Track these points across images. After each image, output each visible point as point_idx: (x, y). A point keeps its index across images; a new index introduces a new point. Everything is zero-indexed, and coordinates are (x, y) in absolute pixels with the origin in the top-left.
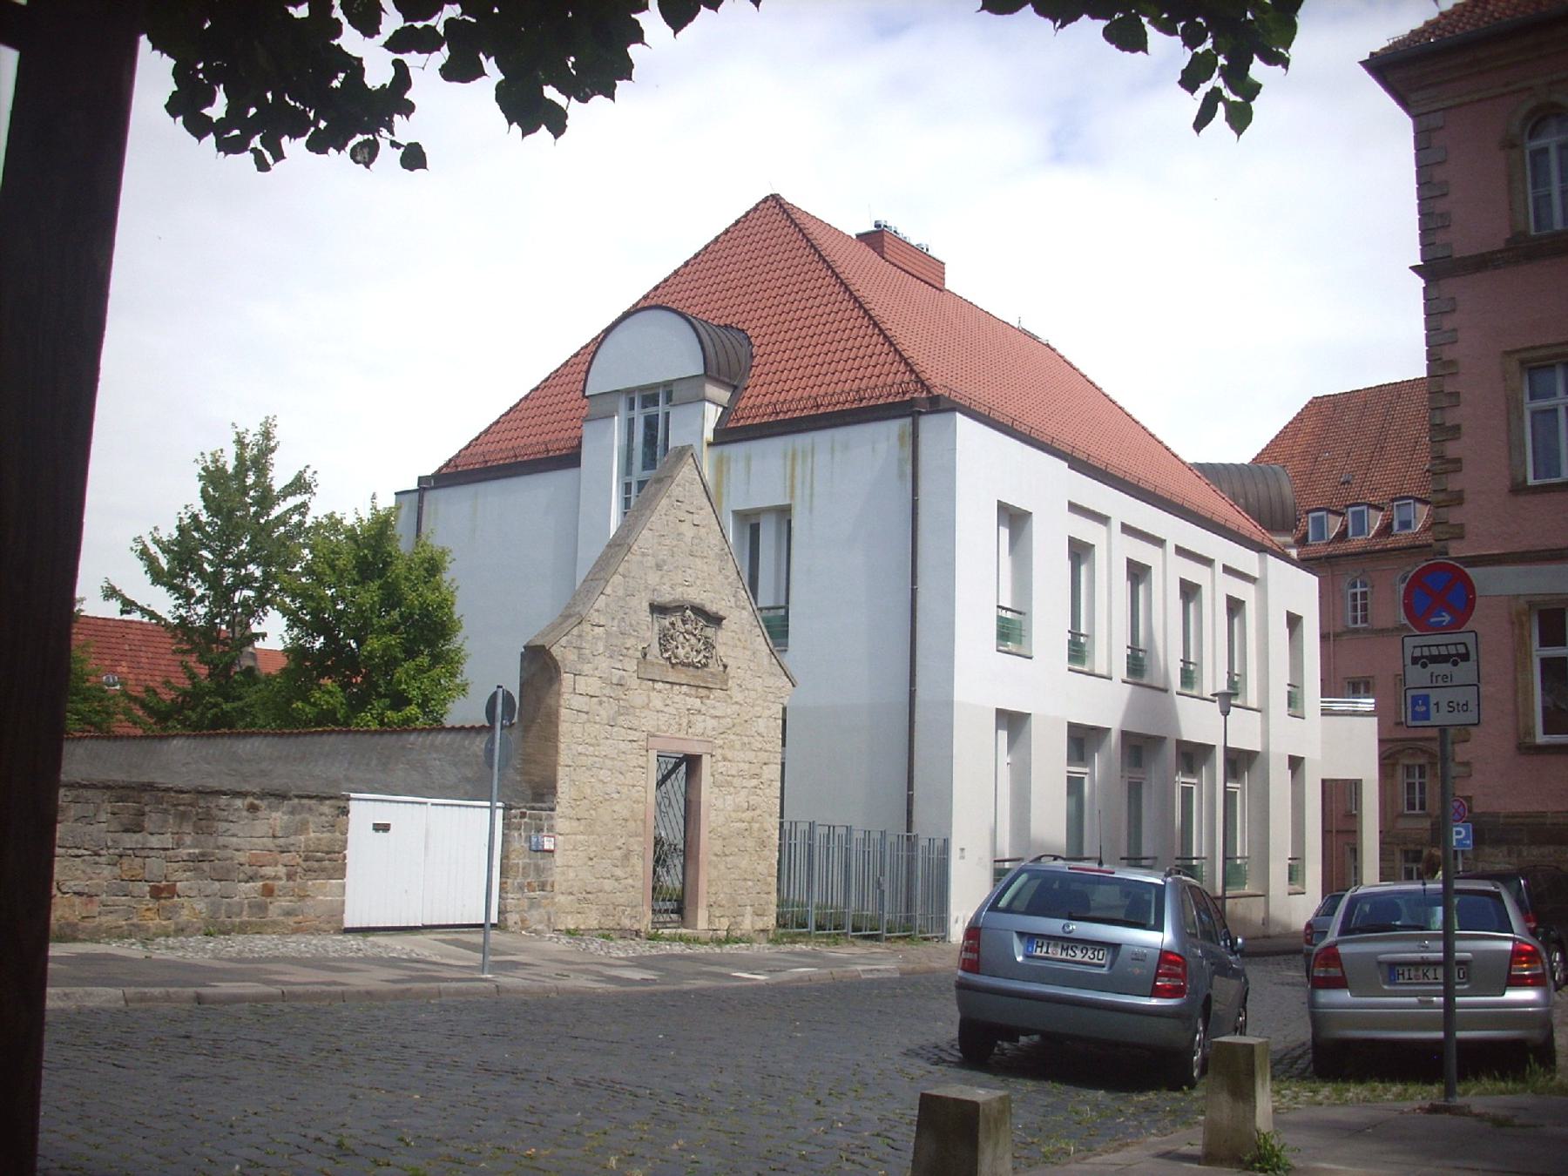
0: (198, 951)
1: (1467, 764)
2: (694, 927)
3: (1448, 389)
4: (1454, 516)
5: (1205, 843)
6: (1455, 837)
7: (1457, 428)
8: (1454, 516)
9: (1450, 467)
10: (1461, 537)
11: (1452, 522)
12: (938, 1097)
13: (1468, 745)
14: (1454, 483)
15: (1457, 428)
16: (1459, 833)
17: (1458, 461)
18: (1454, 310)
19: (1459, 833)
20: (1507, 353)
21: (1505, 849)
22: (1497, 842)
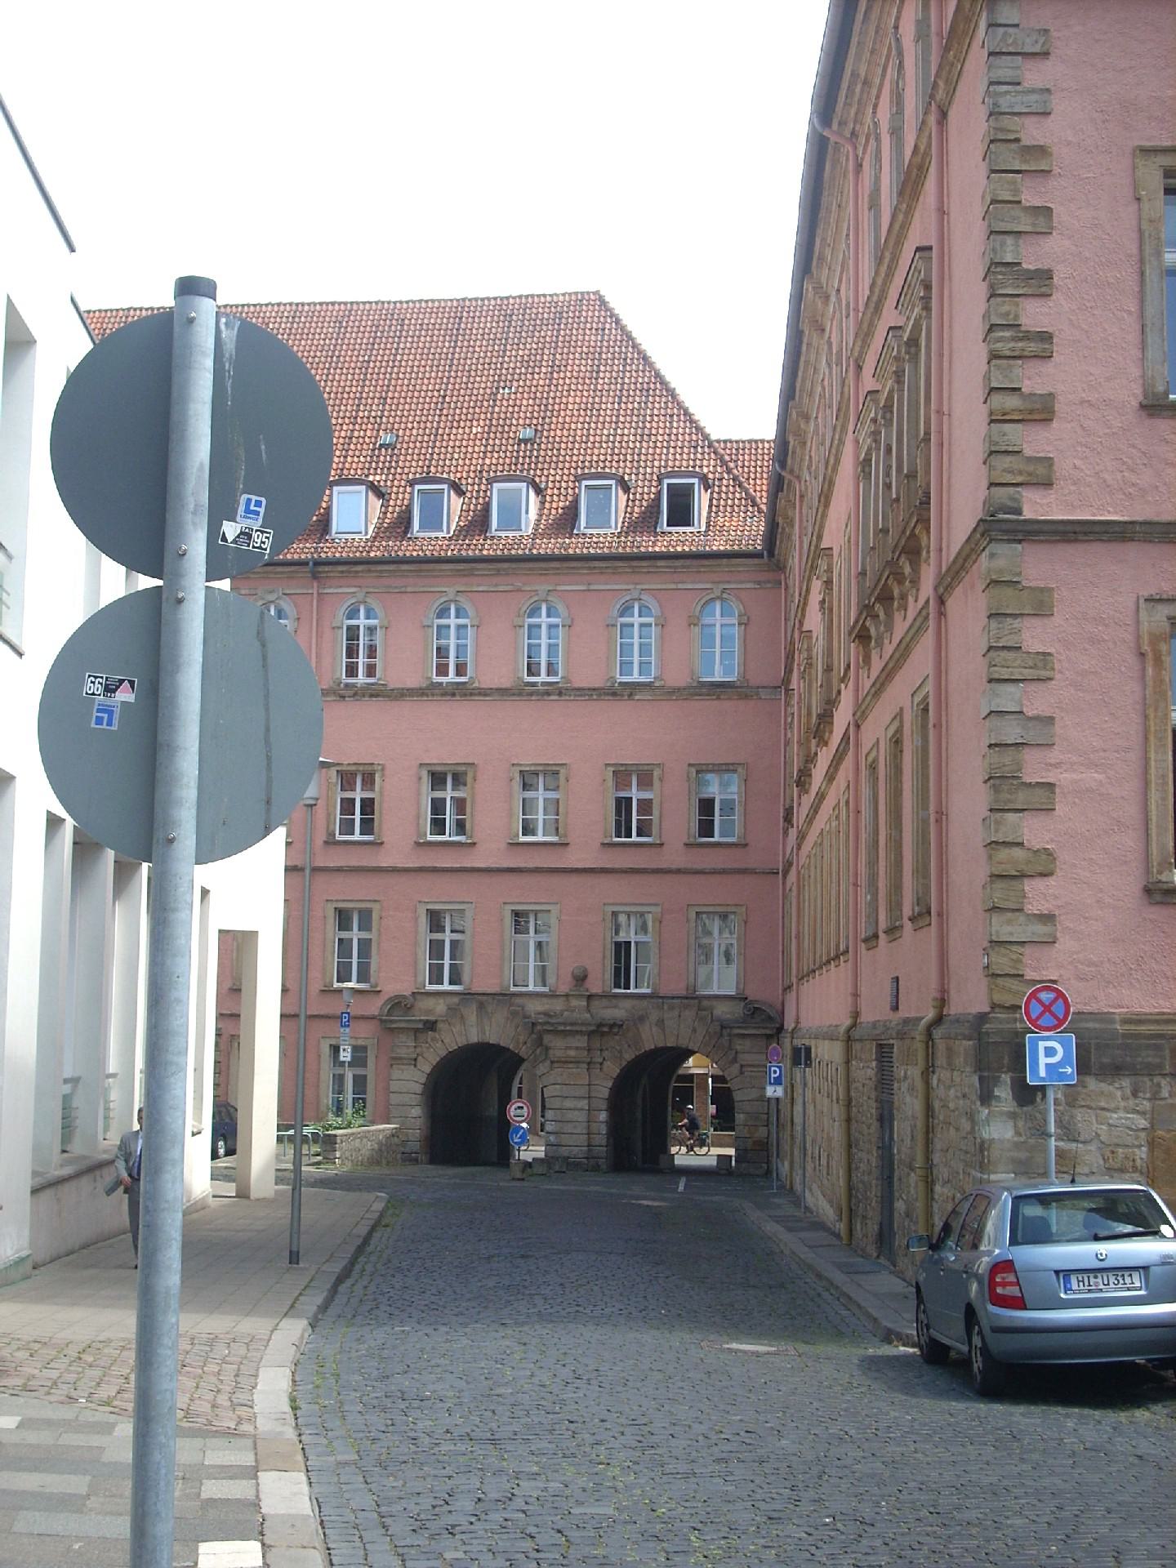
0: (770, 1227)
1: (1048, 918)
2: (184, 1305)
3: (1029, 198)
4: (1034, 441)
5: (824, 281)
6: (1043, 1060)
7: (1046, 275)
8: (1034, 441)
9: (1032, 347)
10: (1048, 484)
11: (1028, 452)
12: (466, 1165)
13: (1051, 881)
14: (1034, 379)
15: (1046, 275)
16: (1050, 1052)
17: (1046, 337)
18: (1046, 54)
19: (1050, 1052)
20: (1146, 151)
21: (1126, 1083)
22: (1114, 1071)
